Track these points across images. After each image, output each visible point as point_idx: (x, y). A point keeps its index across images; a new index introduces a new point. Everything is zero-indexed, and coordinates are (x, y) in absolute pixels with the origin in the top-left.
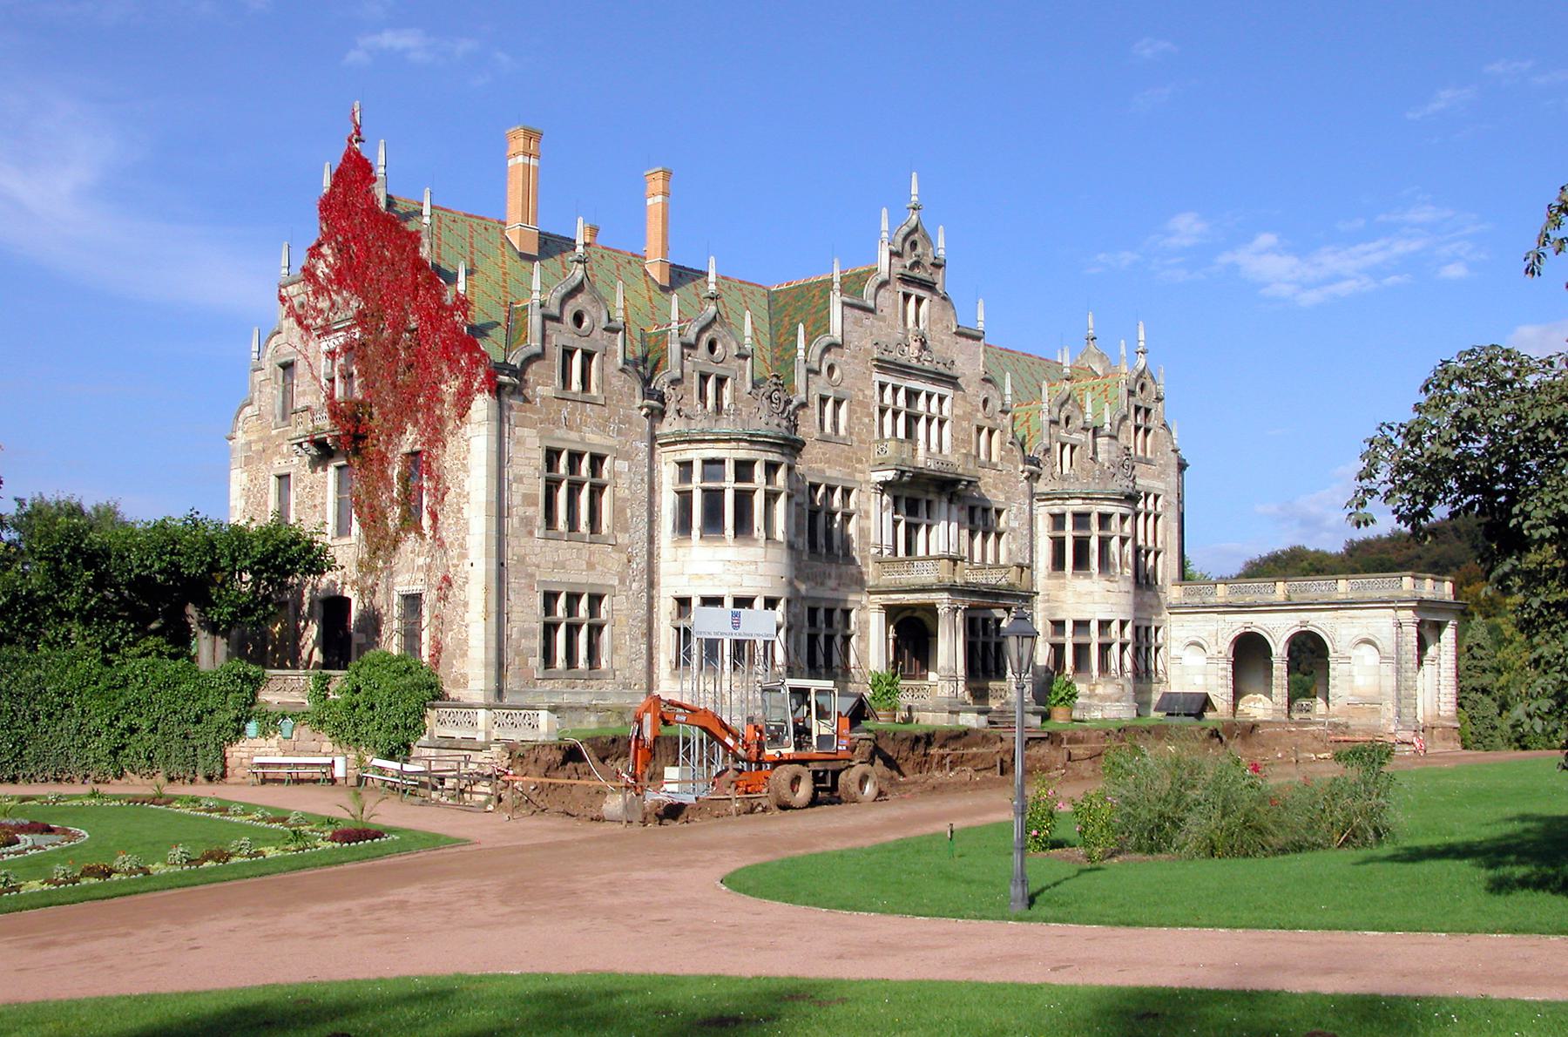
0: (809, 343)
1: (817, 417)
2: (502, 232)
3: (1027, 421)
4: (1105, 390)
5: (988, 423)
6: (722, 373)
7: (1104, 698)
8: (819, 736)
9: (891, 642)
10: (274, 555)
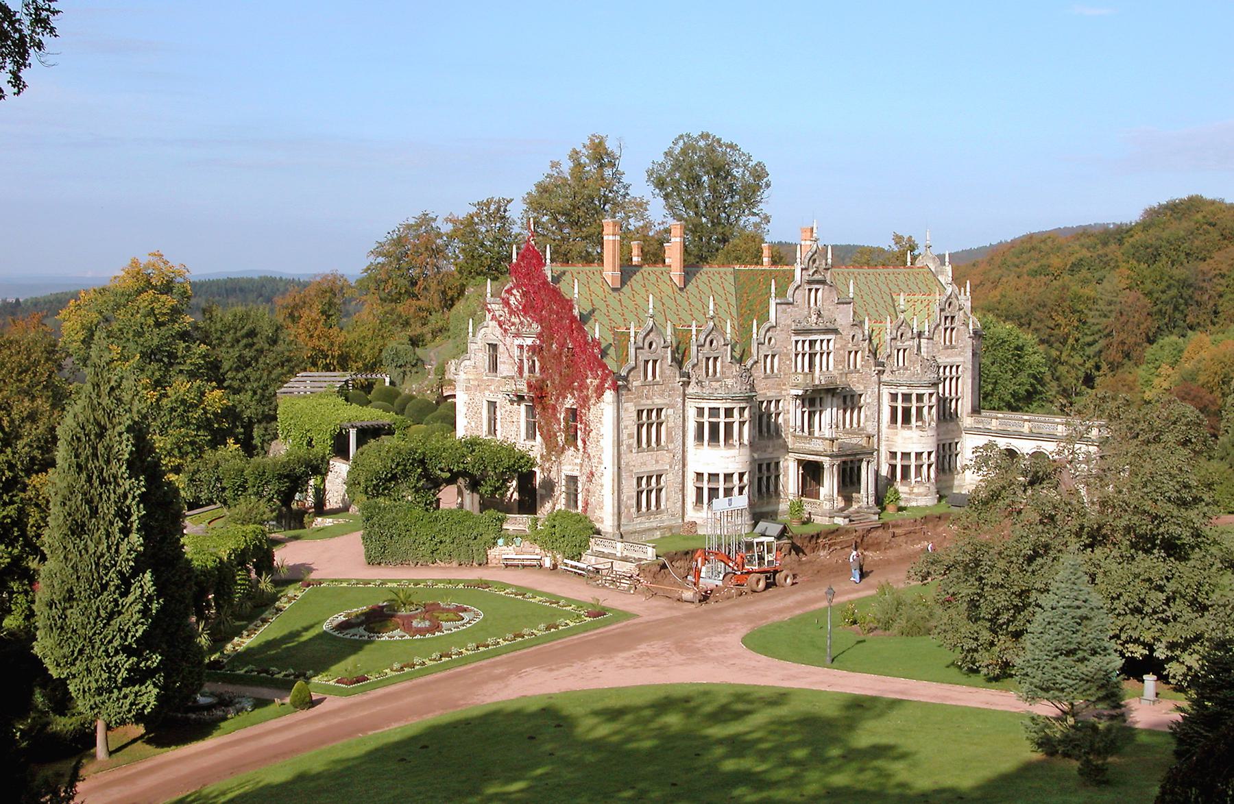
0: (758, 328)
1: (763, 367)
2: (601, 273)
3: (879, 334)
4: (928, 305)
5: (855, 348)
6: (716, 355)
7: (919, 495)
8: (768, 561)
9: (800, 475)
10: (514, 465)
